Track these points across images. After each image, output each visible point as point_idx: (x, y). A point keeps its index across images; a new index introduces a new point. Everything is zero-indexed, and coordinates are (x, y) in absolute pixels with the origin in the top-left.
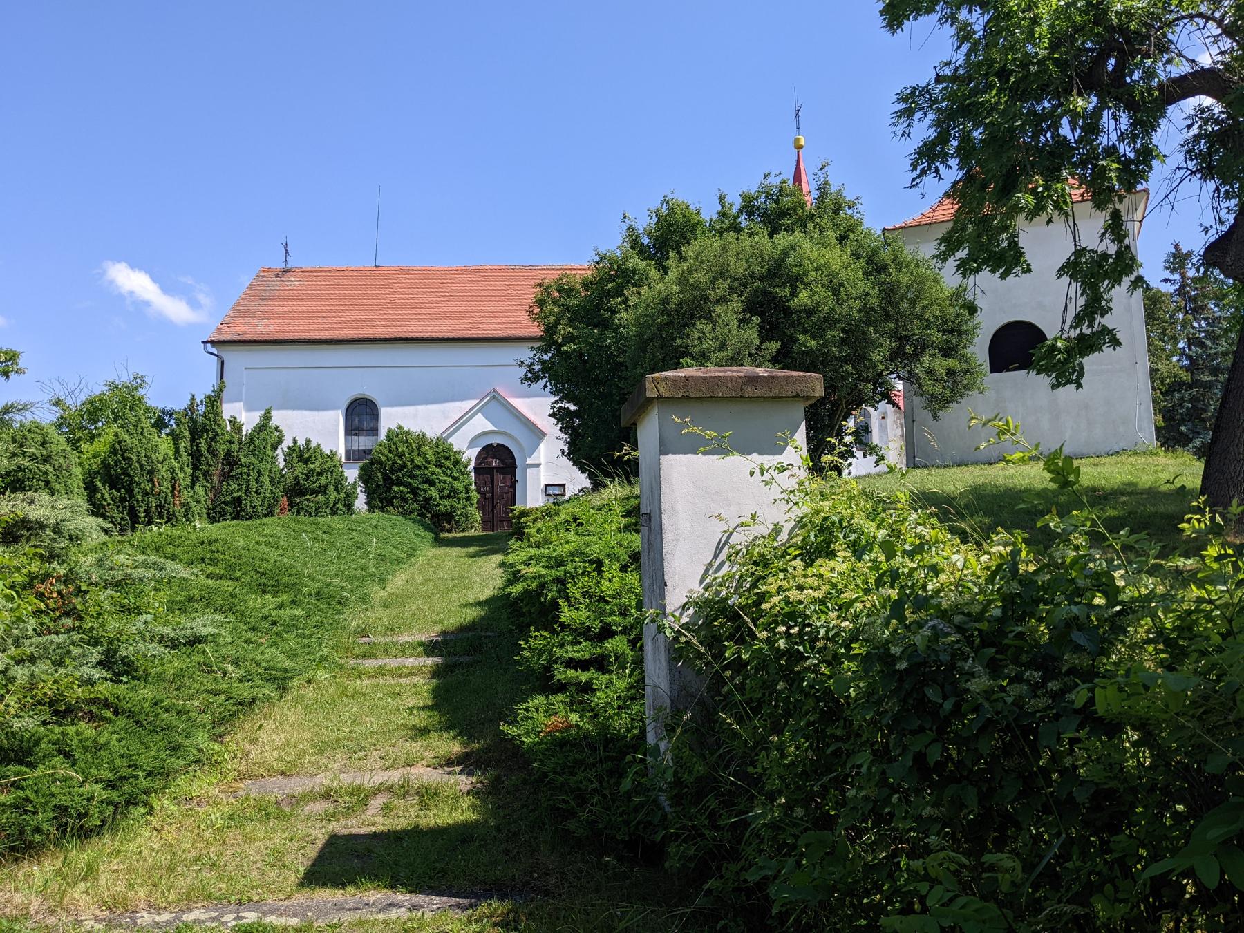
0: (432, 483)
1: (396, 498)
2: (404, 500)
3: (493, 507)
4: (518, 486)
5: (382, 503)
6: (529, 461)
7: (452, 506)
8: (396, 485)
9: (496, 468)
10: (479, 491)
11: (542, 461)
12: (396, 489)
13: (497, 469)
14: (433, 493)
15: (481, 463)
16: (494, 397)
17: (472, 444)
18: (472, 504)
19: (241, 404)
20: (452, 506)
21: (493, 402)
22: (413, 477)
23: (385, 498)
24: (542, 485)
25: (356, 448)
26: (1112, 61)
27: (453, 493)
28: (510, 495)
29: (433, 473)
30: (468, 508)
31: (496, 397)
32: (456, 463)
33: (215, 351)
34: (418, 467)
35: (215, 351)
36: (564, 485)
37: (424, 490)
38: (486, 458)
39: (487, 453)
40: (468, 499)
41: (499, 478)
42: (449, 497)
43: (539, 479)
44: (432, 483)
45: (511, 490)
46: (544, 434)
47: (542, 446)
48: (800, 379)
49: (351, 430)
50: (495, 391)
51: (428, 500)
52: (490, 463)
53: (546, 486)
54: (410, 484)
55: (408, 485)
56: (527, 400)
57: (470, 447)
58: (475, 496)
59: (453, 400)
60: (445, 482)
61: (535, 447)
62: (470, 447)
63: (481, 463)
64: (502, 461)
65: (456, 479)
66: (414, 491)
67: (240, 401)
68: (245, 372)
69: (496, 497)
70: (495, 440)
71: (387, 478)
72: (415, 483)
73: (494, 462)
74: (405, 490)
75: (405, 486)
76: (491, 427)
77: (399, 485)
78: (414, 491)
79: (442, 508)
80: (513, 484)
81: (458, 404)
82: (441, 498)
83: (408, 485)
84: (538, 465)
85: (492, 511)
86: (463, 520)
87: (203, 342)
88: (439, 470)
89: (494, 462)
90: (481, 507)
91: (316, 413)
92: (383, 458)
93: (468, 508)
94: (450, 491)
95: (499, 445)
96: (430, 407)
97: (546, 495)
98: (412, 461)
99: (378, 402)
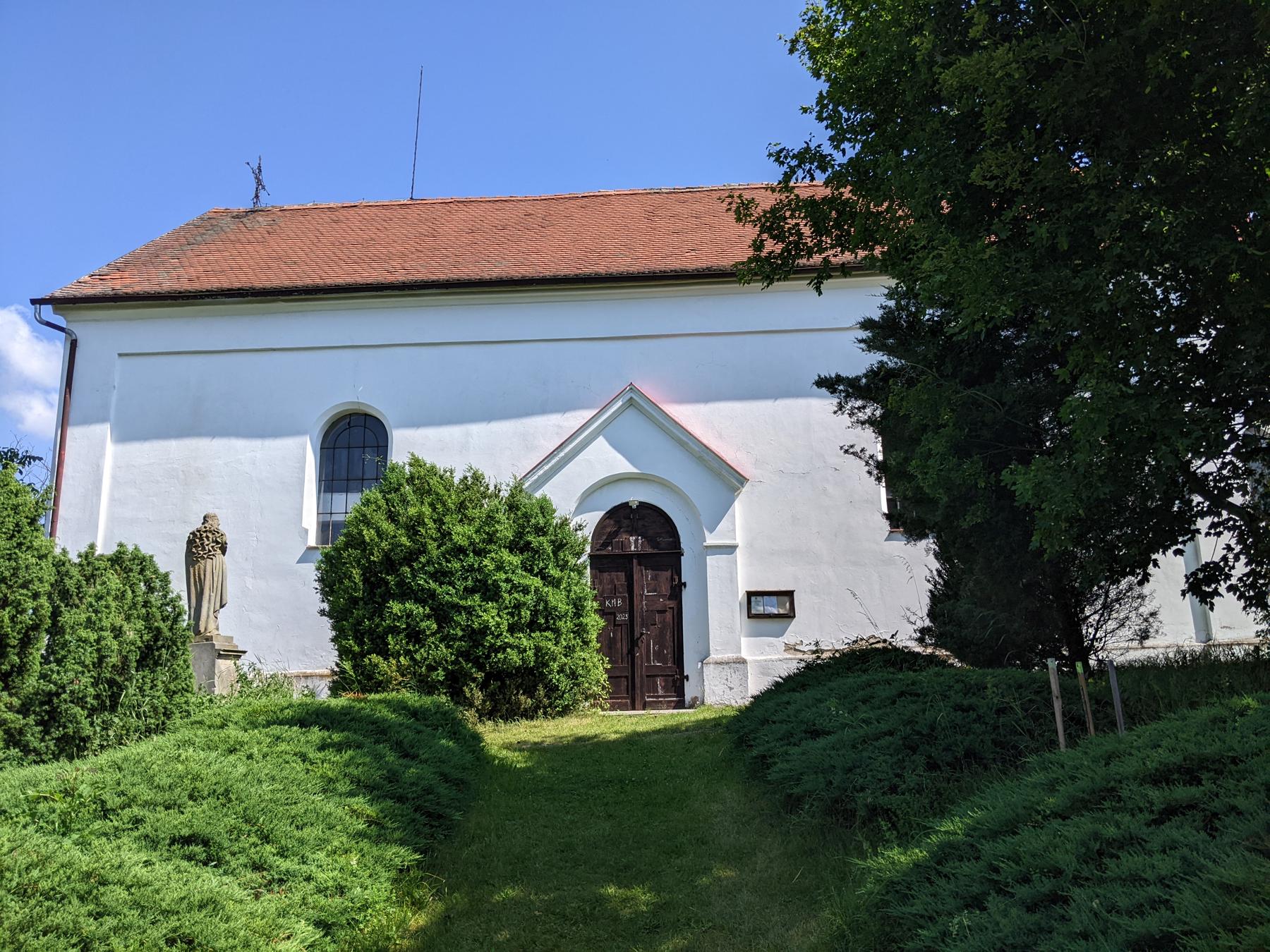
0: (490, 592)
1: (394, 630)
2: (416, 636)
3: (633, 643)
4: (687, 596)
5: (361, 644)
6: (711, 540)
7: (538, 649)
8: (394, 597)
9: (639, 556)
10: (602, 612)
11: (739, 540)
12: (396, 607)
13: (641, 557)
14: (491, 616)
15: (605, 545)
16: (631, 403)
17: (585, 502)
18: (586, 643)
19: (105, 429)
20: (538, 649)
21: (631, 414)
22: (441, 576)
23: (371, 632)
24: (741, 594)
25: (340, 518)
26: (1208, 155)
27: (543, 619)
28: (669, 615)
29: (500, 567)
30: (579, 654)
31: (635, 402)
32: (559, 546)
33: (59, 320)
34: (459, 551)
35: (59, 320)
36: (790, 594)
37: (469, 611)
38: (616, 534)
39: (618, 522)
40: (580, 630)
41: (644, 577)
42: (533, 626)
43: (733, 580)
44: (490, 592)
45: (671, 604)
46: (742, 480)
47: (738, 506)
48: (318, 668)
49: (331, 481)
50: (632, 388)
51: (477, 635)
52: (623, 545)
53: (750, 595)
54: (432, 594)
55: (426, 597)
56: (702, 408)
57: (580, 510)
58: (594, 622)
59: (544, 410)
60: (526, 591)
61: (725, 507)
62: (580, 510)
63: (605, 545)
64: (650, 540)
65: (555, 583)
66: (442, 614)
67: (103, 420)
68: (119, 362)
69: (638, 621)
70: (635, 495)
71: (373, 580)
72: (447, 593)
73: (634, 544)
74: (418, 610)
75: (417, 601)
76: (625, 467)
77: (402, 598)
78: (442, 614)
79: (514, 657)
80: (677, 589)
81: (554, 419)
82: (512, 629)
83: (426, 597)
84: (731, 549)
85: (631, 652)
86: (564, 683)
87: (34, 302)
88: (516, 560)
89: (634, 544)
90: (608, 647)
91: (257, 443)
92: (368, 534)
93: (579, 654)
94: (535, 613)
95: (643, 505)
96: (496, 426)
97: (750, 616)
98: (446, 535)
99: (388, 418)
